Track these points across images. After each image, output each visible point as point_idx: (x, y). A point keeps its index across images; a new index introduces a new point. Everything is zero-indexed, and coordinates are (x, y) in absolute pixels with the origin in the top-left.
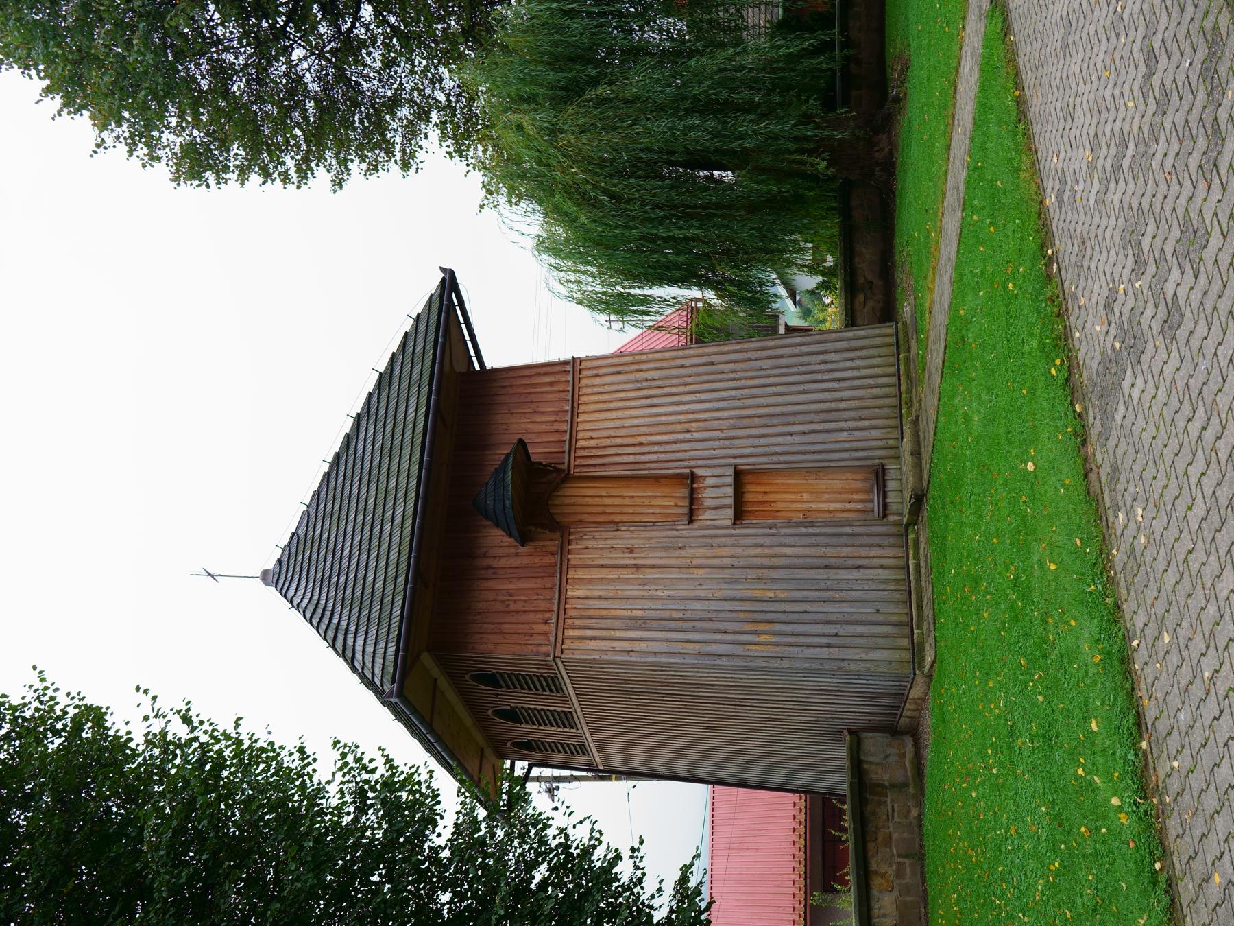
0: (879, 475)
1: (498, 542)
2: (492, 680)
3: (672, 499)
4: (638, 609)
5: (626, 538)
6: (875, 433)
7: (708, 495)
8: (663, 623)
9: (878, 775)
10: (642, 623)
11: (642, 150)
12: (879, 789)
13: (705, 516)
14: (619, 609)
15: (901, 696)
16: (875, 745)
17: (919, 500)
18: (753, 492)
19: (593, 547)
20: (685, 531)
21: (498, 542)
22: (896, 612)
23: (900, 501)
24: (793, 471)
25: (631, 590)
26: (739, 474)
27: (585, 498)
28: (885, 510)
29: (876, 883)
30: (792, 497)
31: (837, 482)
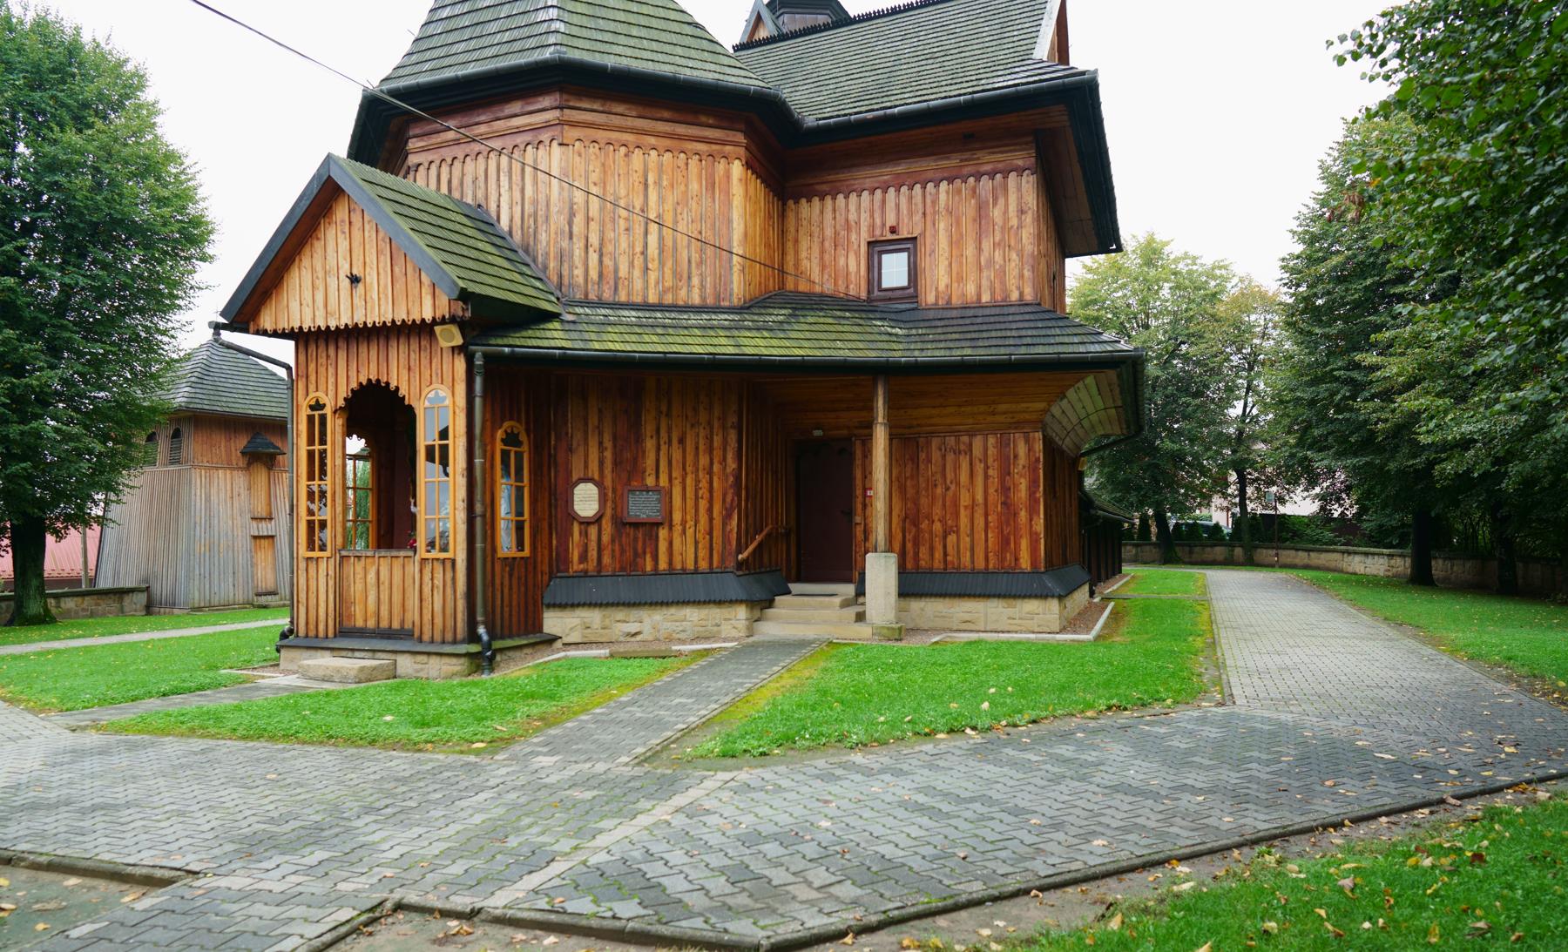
0: (274, 593)
1: (242, 442)
2: (177, 434)
3: (261, 510)
4: (214, 498)
5: (244, 493)
6: (579, 272)
7: (263, 525)
8: (208, 508)
9: (127, 599)
10: (208, 499)
11: (839, 778)
12: (121, 601)
13: (254, 523)
14: (214, 491)
15: (173, 605)
16: (141, 598)
17: (265, 607)
18: (265, 543)
19: (240, 479)
20: (248, 516)
21: (242, 442)
22: (215, 601)
23: (263, 600)
24: (275, 559)
25: (222, 496)
26: (272, 537)
27: (261, 475)
28: (259, 595)
29: (79, 599)
30: (264, 558)
31: (270, 576)
